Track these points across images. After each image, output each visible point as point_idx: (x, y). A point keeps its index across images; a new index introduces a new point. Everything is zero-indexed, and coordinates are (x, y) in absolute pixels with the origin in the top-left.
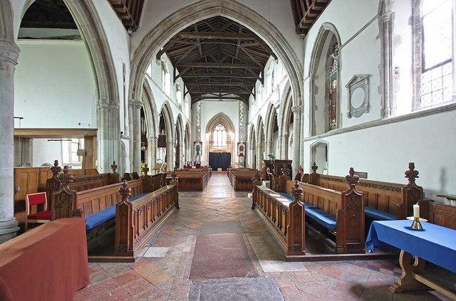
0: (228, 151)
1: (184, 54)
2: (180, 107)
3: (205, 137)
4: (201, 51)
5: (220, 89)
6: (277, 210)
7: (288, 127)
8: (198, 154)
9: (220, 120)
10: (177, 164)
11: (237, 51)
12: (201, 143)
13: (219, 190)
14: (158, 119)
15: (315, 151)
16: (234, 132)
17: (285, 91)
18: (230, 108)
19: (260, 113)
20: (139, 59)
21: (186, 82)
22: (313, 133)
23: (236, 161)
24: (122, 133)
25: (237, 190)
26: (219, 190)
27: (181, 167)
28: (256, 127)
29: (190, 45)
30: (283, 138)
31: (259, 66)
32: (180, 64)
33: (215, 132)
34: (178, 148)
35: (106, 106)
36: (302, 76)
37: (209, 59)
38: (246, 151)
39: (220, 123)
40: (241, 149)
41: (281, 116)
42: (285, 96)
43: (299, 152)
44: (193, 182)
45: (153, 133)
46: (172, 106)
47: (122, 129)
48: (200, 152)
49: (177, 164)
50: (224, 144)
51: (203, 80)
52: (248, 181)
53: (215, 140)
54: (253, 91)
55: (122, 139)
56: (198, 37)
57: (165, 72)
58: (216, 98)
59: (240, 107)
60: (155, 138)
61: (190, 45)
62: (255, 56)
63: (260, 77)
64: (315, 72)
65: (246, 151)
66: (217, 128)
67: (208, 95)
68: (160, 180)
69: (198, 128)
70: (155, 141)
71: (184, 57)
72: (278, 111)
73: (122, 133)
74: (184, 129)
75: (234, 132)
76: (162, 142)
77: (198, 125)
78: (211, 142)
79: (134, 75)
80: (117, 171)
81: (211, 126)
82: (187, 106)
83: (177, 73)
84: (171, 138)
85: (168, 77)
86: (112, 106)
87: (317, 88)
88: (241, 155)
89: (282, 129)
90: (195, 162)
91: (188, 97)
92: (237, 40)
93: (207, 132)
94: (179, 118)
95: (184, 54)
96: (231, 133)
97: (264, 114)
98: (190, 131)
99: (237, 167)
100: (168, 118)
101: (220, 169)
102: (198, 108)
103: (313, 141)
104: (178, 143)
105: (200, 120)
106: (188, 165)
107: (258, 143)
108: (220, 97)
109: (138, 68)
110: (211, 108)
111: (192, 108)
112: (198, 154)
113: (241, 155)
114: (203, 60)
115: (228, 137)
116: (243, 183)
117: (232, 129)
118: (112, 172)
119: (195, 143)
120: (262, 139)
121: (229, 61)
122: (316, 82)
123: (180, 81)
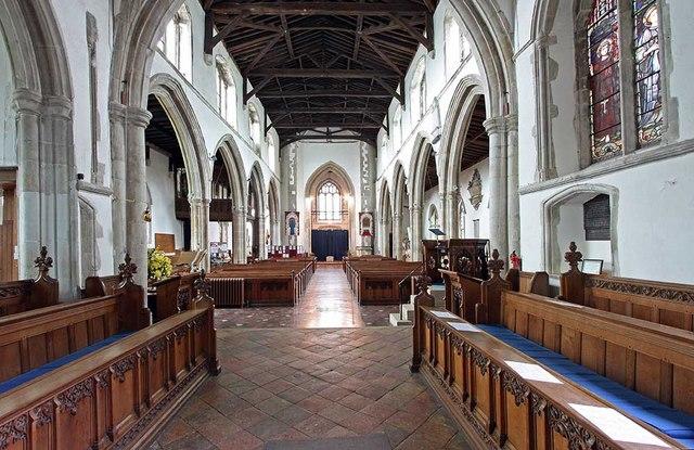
0: (344, 227)
1: (261, 50)
2: (258, 151)
3: (303, 204)
4: (290, 46)
5: (329, 120)
6: (428, 331)
7: (458, 178)
8: (292, 233)
9: (329, 175)
10: (256, 250)
11: (357, 45)
12: (298, 214)
13: (330, 305)
14: (246, 185)
15: (557, 215)
16: (353, 194)
17: (451, 106)
18: (345, 153)
19: (400, 157)
20: (135, 17)
21: (270, 107)
22: (549, 171)
23: (357, 242)
24: (80, 176)
25: (364, 302)
26: (330, 305)
27: (264, 255)
28: (391, 185)
29: (272, 33)
30: (449, 198)
31: (396, 73)
32: (257, 71)
33: (322, 196)
34: (256, 223)
35: (31, 105)
36: (509, 46)
37: (308, 65)
38: (373, 228)
39: (329, 180)
40: (366, 222)
41: (444, 156)
42: (452, 116)
43: (506, 218)
44: (274, 288)
45: (201, 192)
46: (240, 145)
47: (83, 165)
48: (296, 229)
49: (256, 250)
50: (338, 216)
51: (298, 105)
52: (386, 283)
53: (322, 207)
54: (385, 123)
55: (81, 193)
56: (283, 12)
57: (227, 84)
58: (322, 137)
59: (362, 151)
60: (204, 201)
61: (272, 33)
62: (388, 52)
63: (398, 91)
64: (550, 21)
65: (373, 228)
66: (324, 189)
67: (308, 133)
68: (171, 294)
69: (293, 188)
70: (205, 208)
71: (260, 57)
72: (436, 147)
73: (80, 176)
74: (267, 187)
75: (353, 194)
76: (221, 211)
77: (292, 183)
78: (315, 212)
79: (125, 49)
80: (51, 273)
81: (314, 186)
82: (271, 153)
83: (250, 88)
84: (241, 204)
85: (232, 95)
86: (51, 110)
87: (555, 65)
88: (366, 233)
89: (446, 182)
90: (287, 248)
91: (273, 135)
92: (356, 17)
93: (308, 194)
94: (256, 168)
95: (261, 50)
96: (347, 197)
97: (406, 160)
98: (278, 193)
99: (359, 254)
100: (233, 165)
101: (330, 259)
102: (292, 155)
103: (553, 191)
104: (257, 213)
105: (295, 175)
106: (276, 252)
107: (396, 212)
108: (329, 136)
109: (136, 34)
110: (313, 154)
111: (281, 155)
112: (292, 233)
113: (366, 233)
114: (295, 65)
115: (343, 205)
116: (378, 288)
117: (350, 189)
118: (37, 278)
119: (287, 213)
120: (404, 206)
121: (342, 65)
122: (553, 52)
123: (255, 102)
